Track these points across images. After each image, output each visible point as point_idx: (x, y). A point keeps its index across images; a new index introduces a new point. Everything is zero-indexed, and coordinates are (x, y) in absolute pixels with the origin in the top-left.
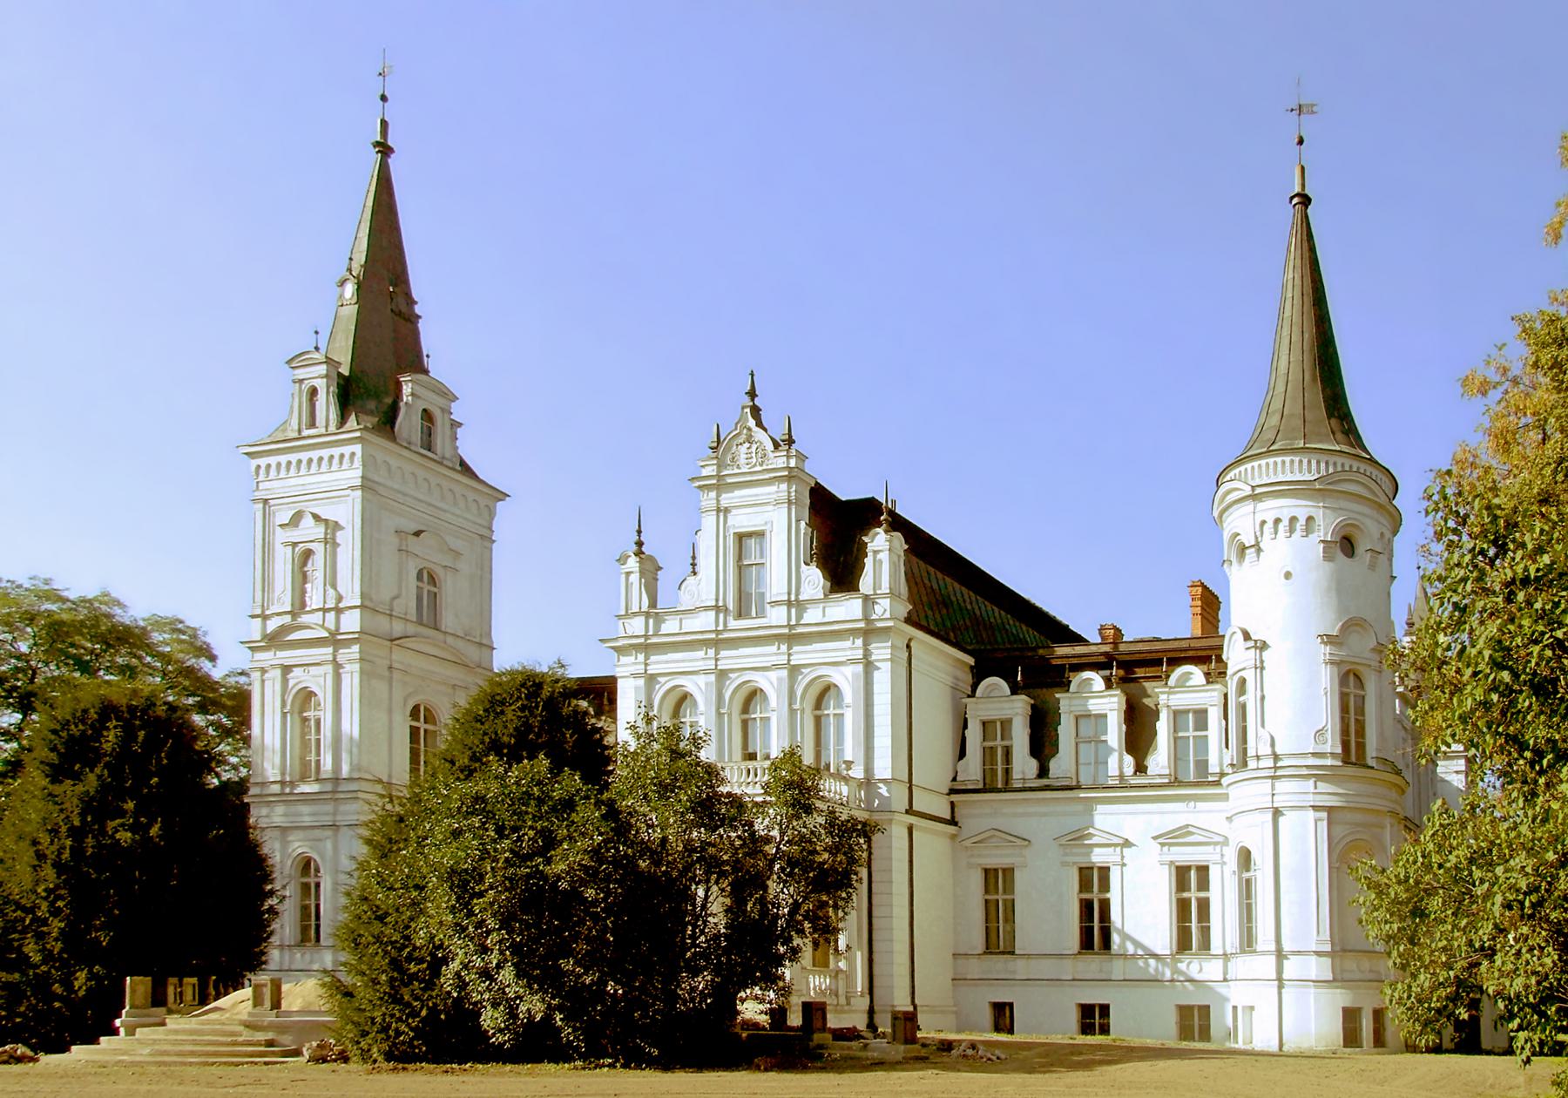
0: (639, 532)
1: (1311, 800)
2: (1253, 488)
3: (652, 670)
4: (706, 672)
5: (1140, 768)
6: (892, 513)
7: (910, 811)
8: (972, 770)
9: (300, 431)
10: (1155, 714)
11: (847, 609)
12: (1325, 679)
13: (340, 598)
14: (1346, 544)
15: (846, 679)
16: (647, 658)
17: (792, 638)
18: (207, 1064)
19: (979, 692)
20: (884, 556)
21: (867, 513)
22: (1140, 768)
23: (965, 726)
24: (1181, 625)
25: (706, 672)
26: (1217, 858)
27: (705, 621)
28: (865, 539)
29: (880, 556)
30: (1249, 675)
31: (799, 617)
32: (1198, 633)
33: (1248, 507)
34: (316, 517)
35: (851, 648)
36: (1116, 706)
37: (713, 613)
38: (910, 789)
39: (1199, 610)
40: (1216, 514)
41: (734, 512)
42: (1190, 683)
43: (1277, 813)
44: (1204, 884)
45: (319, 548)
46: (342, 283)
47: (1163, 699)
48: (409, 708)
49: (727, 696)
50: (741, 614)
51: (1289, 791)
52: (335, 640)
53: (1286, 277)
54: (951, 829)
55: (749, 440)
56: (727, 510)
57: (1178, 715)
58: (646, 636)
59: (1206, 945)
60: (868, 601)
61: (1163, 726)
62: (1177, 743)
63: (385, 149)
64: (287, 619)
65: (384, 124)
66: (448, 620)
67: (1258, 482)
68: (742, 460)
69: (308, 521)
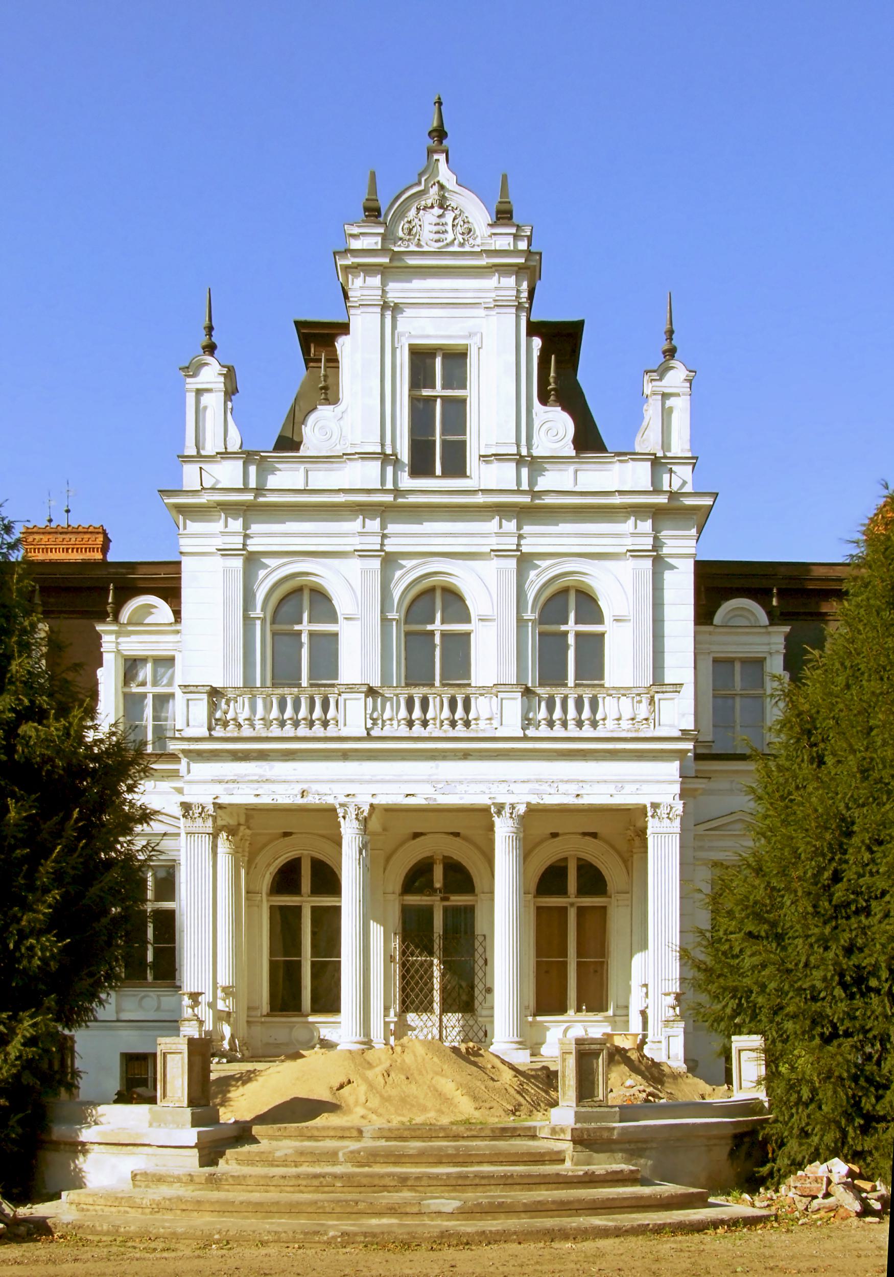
0: (210, 329)
3: (254, 545)
4: (363, 554)
16: (246, 527)
17: (531, 511)
18: (552, 1235)
19: (718, 618)
25: (363, 554)
27: (366, 475)
29: (206, 399)
31: (532, 482)
35: (635, 533)
37: (378, 464)
41: (408, 312)
49: (397, 594)
50: (421, 465)
56: (396, 309)
57: (131, 667)
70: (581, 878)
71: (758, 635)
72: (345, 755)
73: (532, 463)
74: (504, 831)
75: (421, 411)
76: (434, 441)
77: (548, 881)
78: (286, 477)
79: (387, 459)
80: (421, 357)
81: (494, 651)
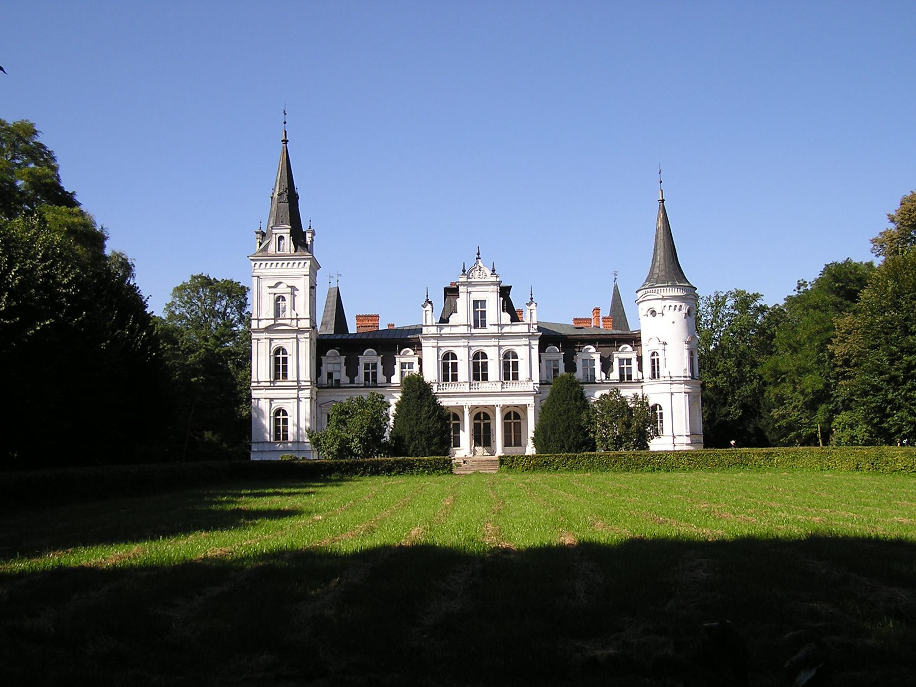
1: (683, 390)
12: (686, 353)
14: (688, 314)
17: (502, 336)
27: (463, 330)
35: (525, 341)
43: (672, 394)
45: (288, 297)
50: (476, 326)
51: (676, 388)
52: (299, 331)
53: (653, 224)
57: (621, 361)
64: (272, 322)
68: (477, 276)
70: (513, 417)
71: (556, 353)
72: (465, 396)
73: (501, 326)
74: (498, 410)
75: (476, 313)
76: (479, 319)
77: (507, 417)
78: (446, 330)
79: (469, 326)
80: (476, 303)
81: (494, 370)
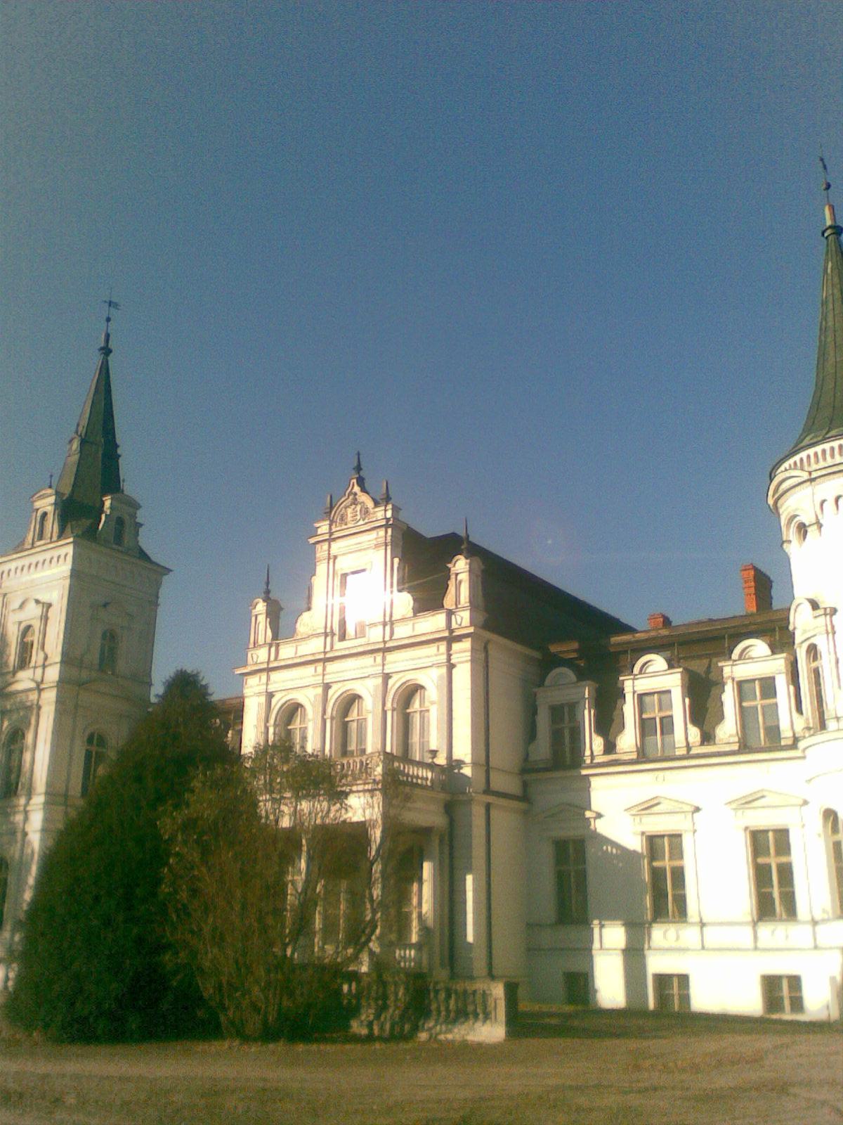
0: (268, 583)
2: (810, 473)
5: (707, 738)
6: (470, 543)
7: (488, 791)
8: (542, 748)
9: (33, 543)
10: (721, 684)
11: (434, 622)
13: (46, 658)
15: (431, 680)
19: (547, 682)
20: (464, 577)
21: (451, 545)
22: (707, 738)
23: (535, 713)
24: (740, 604)
25: (315, 686)
26: (690, 826)
28: (449, 565)
30: (822, 643)
32: (754, 610)
33: (806, 490)
34: (37, 602)
35: (436, 653)
36: (783, 668)
38: (488, 772)
39: (753, 591)
40: (771, 501)
42: (650, 670)
44: (677, 852)
46: (71, 441)
47: (727, 671)
48: (87, 734)
54: (522, 805)
55: (355, 502)
57: (742, 687)
58: (325, 653)
59: (791, 911)
60: (450, 614)
61: (729, 697)
62: (745, 715)
63: (106, 351)
65: (108, 336)
66: (122, 666)
67: (814, 467)
69: (32, 605)
